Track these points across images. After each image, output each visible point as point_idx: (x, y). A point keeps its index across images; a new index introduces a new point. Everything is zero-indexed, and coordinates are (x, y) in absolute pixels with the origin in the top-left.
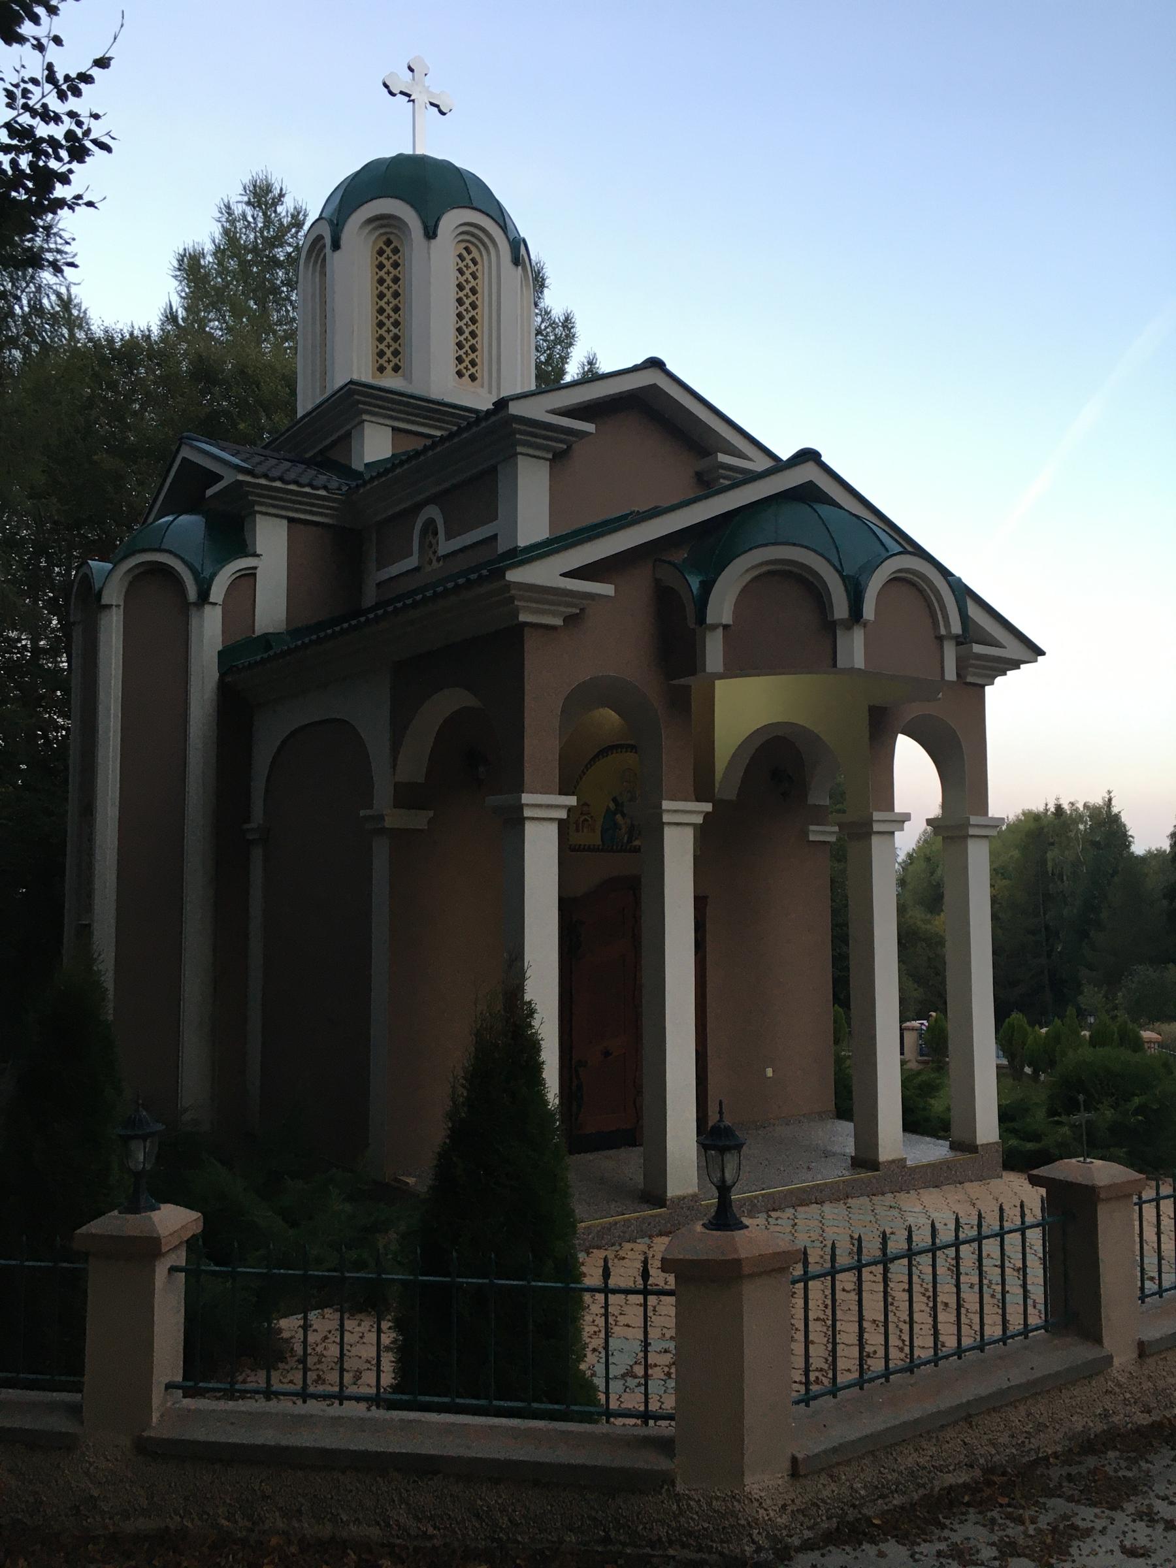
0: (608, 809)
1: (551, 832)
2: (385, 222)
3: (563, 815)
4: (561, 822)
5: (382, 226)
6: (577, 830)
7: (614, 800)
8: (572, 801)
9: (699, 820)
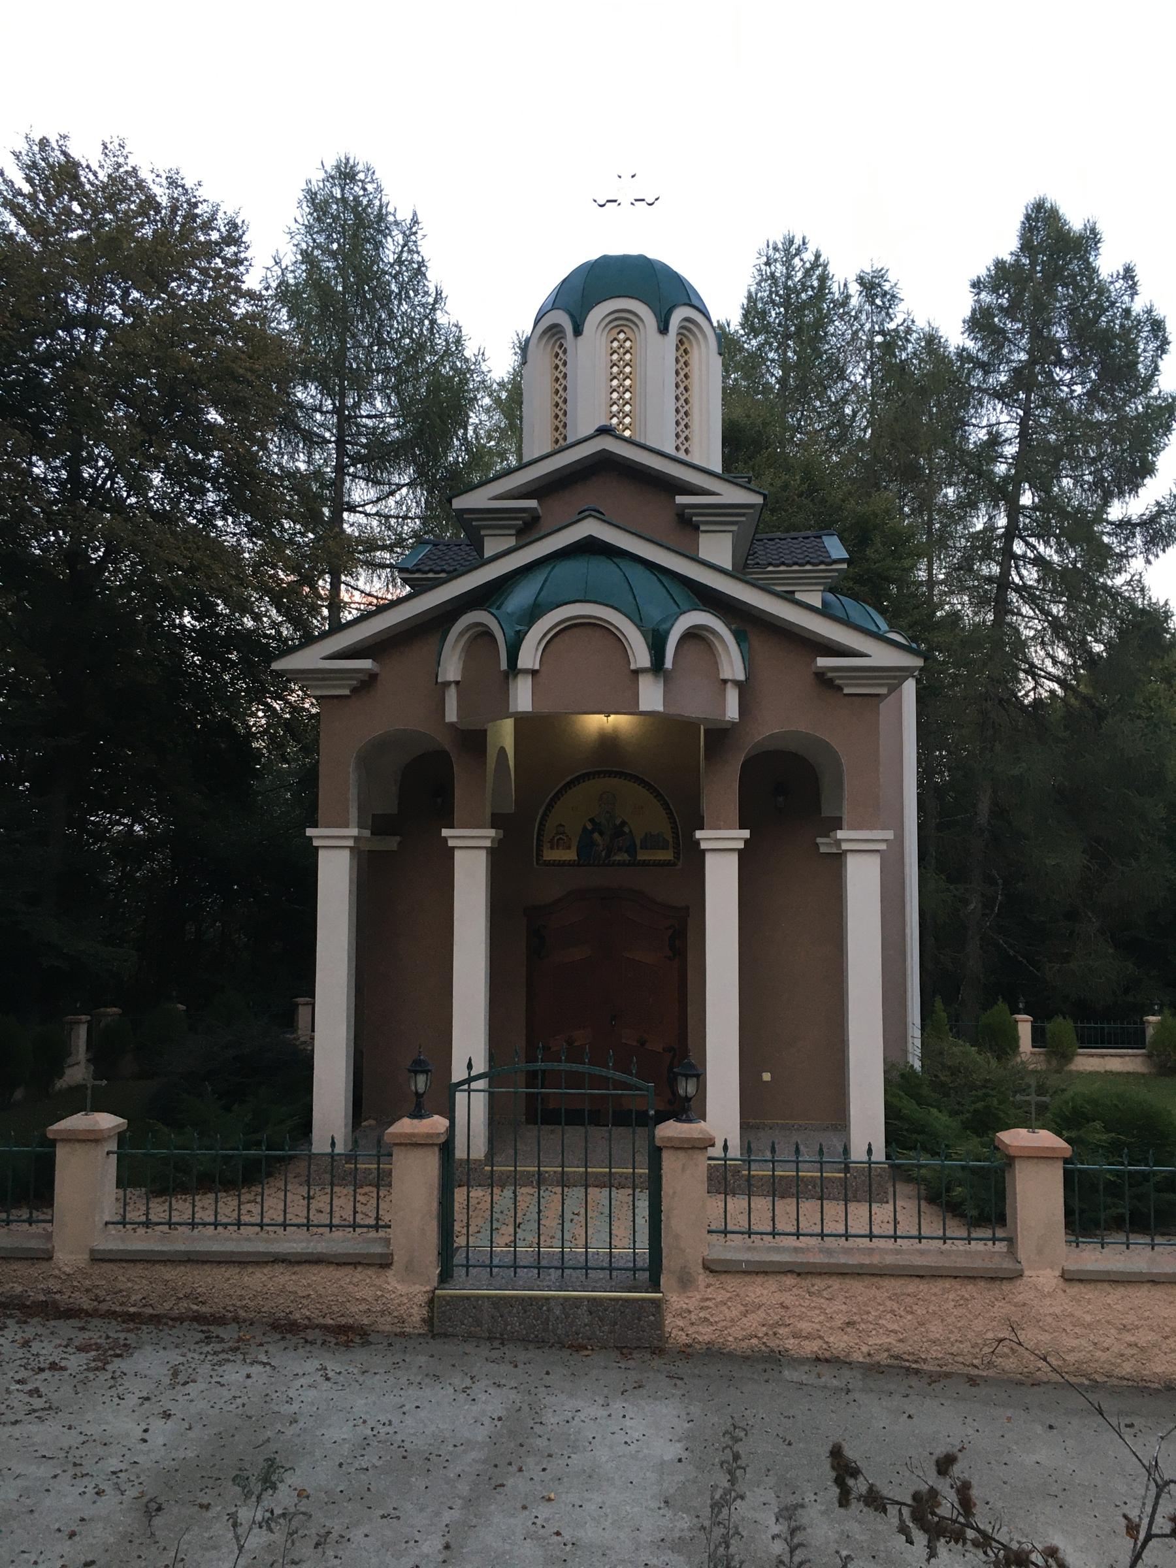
0: (585, 828)
1: (731, 863)
2: (554, 330)
3: (741, 845)
4: (740, 851)
5: (554, 335)
6: (552, 848)
7: (592, 820)
8: (746, 833)
9: (741, 845)
